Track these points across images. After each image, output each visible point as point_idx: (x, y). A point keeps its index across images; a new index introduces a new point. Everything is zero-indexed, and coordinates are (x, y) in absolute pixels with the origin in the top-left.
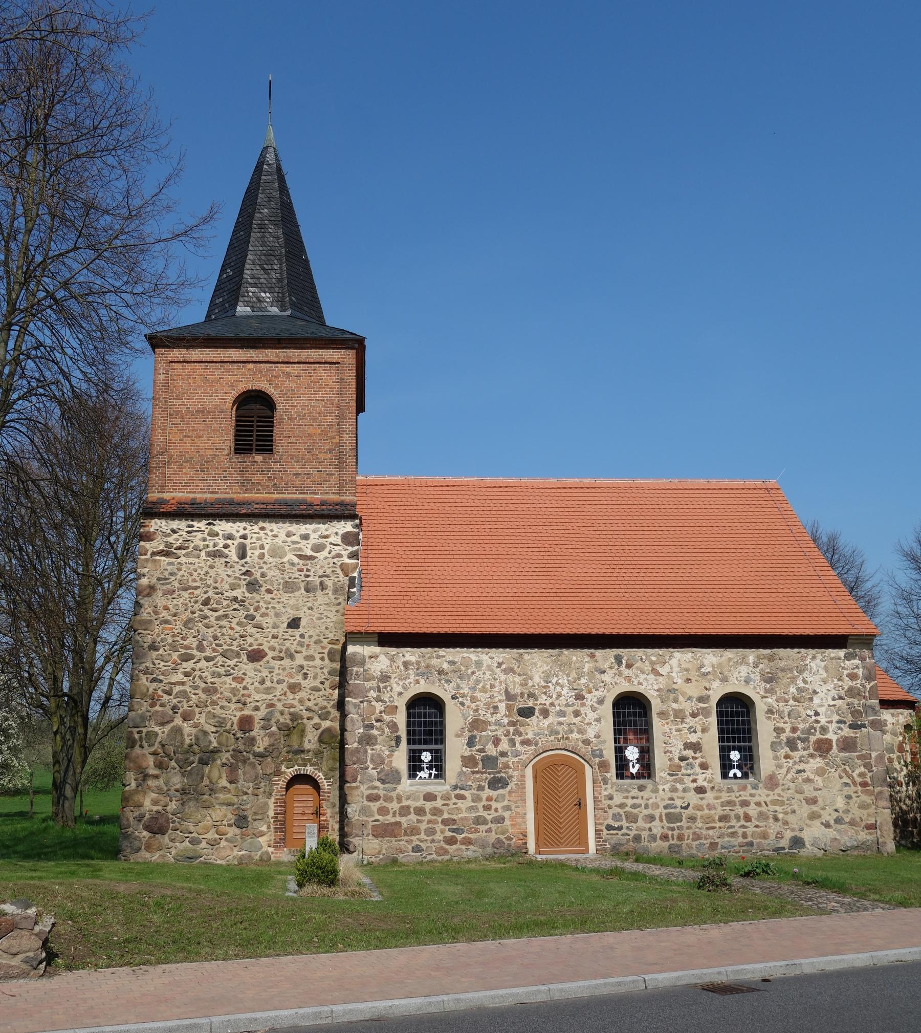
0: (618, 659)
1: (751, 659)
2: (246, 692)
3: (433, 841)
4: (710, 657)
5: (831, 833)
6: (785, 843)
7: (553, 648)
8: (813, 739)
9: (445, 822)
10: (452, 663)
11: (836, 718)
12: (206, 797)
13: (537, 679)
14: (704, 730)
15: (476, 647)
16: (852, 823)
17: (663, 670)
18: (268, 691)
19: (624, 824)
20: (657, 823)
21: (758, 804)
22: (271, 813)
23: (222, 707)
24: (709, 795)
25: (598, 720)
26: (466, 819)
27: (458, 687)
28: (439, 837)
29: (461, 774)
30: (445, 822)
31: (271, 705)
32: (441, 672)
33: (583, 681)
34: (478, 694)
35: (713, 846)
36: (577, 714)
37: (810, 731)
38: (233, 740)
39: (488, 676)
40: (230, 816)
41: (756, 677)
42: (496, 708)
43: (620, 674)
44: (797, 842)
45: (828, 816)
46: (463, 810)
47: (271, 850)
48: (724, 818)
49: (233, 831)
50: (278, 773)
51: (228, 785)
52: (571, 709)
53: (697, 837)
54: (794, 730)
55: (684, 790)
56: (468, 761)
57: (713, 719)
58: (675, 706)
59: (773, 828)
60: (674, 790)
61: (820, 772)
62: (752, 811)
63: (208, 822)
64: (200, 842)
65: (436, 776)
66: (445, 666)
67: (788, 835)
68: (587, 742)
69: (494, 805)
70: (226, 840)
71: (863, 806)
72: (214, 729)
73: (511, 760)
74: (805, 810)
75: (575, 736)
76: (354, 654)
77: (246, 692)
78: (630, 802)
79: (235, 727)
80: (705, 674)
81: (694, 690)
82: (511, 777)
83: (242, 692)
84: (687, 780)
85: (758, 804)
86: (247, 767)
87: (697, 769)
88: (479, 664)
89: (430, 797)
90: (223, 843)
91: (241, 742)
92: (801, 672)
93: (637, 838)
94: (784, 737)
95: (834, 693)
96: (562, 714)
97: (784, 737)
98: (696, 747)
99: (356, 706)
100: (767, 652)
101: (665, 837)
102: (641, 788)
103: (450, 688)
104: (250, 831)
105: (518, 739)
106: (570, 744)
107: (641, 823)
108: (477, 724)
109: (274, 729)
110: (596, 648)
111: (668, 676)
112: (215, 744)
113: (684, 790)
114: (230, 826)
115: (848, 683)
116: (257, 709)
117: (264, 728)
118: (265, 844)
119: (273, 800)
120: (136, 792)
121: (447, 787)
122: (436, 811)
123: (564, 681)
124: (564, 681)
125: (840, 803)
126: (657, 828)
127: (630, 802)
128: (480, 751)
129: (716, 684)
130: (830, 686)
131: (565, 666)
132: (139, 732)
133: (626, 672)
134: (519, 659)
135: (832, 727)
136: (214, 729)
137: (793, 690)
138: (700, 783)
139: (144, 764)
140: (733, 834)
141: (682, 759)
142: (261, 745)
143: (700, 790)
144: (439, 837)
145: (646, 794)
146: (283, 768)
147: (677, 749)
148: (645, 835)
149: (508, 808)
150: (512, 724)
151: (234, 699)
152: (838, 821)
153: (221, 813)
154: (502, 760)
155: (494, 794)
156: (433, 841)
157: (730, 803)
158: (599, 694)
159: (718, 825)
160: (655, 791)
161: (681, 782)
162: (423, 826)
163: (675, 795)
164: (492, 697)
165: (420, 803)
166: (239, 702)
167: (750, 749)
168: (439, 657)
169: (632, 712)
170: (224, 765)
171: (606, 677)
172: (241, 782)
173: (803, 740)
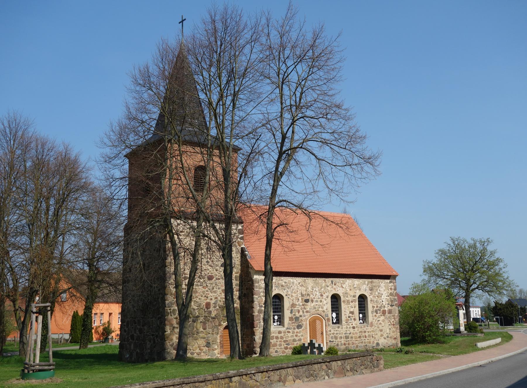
0: (332, 282)
1: (366, 283)
2: (207, 293)
3: (281, 348)
4: (356, 282)
5: (386, 341)
6: (375, 345)
7: (314, 277)
8: (382, 310)
9: (284, 341)
10: (285, 282)
11: (387, 303)
12: (195, 335)
13: (310, 289)
14: (355, 307)
15: (292, 277)
16: (391, 338)
17: (344, 286)
18: (215, 292)
19: (334, 340)
20: (343, 339)
21: (368, 332)
22: (219, 341)
23: (199, 299)
24: (356, 329)
25: (327, 304)
26: (290, 340)
27: (287, 292)
28: (283, 347)
29: (289, 323)
30: (284, 341)
31: (216, 298)
32: (282, 286)
33: (322, 290)
34: (293, 294)
35: (357, 346)
36: (321, 301)
37: (381, 307)
38: (204, 312)
39: (296, 288)
40: (204, 343)
41: (368, 289)
42: (298, 299)
43: (332, 287)
44: (378, 344)
45: (385, 336)
46: (290, 337)
47: (219, 355)
48: (360, 337)
49: (205, 349)
50: (220, 325)
51: (203, 330)
52: (319, 300)
53: (353, 344)
54: (377, 307)
55: (350, 328)
56: (291, 319)
57: (357, 303)
58: (347, 299)
59: (372, 340)
60: (347, 328)
61: (383, 321)
62: (367, 334)
63: (196, 345)
64: (194, 354)
65: (279, 325)
66: (283, 283)
67: (376, 342)
68: (324, 311)
69: (299, 335)
70: (203, 352)
71: (393, 332)
72: (197, 308)
73: (303, 318)
74: (379, 334)
75: (320, 309)
76: (256, 279)
77: (207, 293)
78: (335, 332)
79: (204, 307)
80: (355, 288)
81: (352, 293)
82: (303, 324)
83: (206, 293)
84: (350, 324)
85: (368, 332)
86: (210, 323)
87: (353, 320)
88: (293, 283)
89: (280, 332)
90: (202, 354)
91: (206, 312)
92: (379, 287)
93: (338, 345)
94: (375, 309)
95: (387, 294)
96: (317, 301)
97: (375, 309)
98: (352, 313)
99: (257, 299)
100: (370, 280)
101: (345, 344)
102: (338, 327)
103: (285, 291)
104: (211, 348)
105: (305, 311)
106: (319, 312)
107: (338, 340)
108: (293, 305)
109: (218, 307)
110: (326, 278)
111: (346, 289)
112: (197, 314)
113: (350, 328)
114: (204, 347)
115: (390, 291)
116: (211, 299)
117: (215, 307)
118: (217, 353)
119: (219, 336)
120: (170, 334)
121: (285, 329)
122: (282, 338)
123: (317, 290)
124: (317, 290)
125: (388, 331)
126: (343, 341)
127: (335, 332)
128: (294, 315)
129: (358, 291)
130: (386, 292)
131: (317, 284)
132: (170, 309)
133: (334, 287)
134: (305, 281)
135: (386, 306)
136: (197, 308)
137: (377, 293)
138: (354, 325)
139: (173, 323)
140: (362, 342)
141: (349, 317)
142: (213, 315)
143: (354, 328)
144: (283, 347)
145: (340, 329)
146: (222, 323)
147: (348, 314)
148: (339, 343)
149: (302, 336)
150: (303, 305)
151: (204, 296)
152: (388, 337)
153: (201, 342)
154: (300, 318)
155: (298, 330)
156: (281, 348)
157: (361, 332)
158: (326, 294)
159: (358, 339)
160: (342, 328)
161: (349, 325)
162: (278, 343)
163: (347, 329)
164: (297, 295)
165: (277, 335)
166: (205, 296)
167: (365, 313)
168: (282, 280)
169: (335, 299)
170: (201, 322)
171: (329, 288)
172: (207, 329)
173: (380, 310)
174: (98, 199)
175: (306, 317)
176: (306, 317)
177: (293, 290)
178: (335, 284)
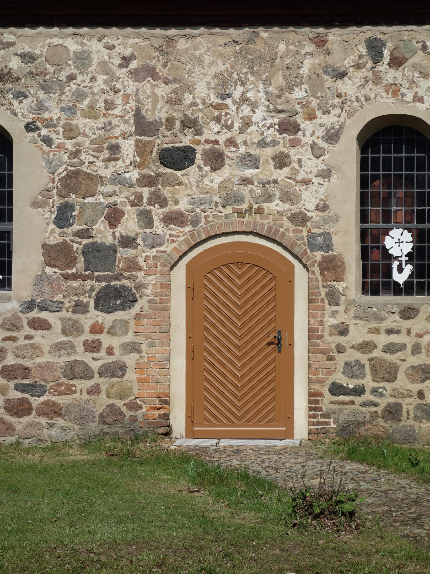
0: (375, 49)
10: (27, 58)
19: (368, 382)
25: (325, 174)
26: (48, 366)
29: (41, 280)
33: (298, 94)
34: (80, 122)
36: (281, 161)
39: (100, 83)
42: (115, 149)
43: (377, 79)
68: (299, 219)
69: (106, 340)
78: (382, 340)
82: (141, 287)
88: (83, 60)
96: (251, 161)
105: (157, 212)
108: (76, 181)
128: (83, 234)
133: (390, 75)
145: (416, 324)
148: (409, 405)
149: (133, 348)
154: (124, 253)
155: (106, 319)
158: (330, 120)
171: (347, 87)
174: (275, 46)
175: (167, 248)
176: (167, 248)
177: (79, 96)
178: (396, 62)
